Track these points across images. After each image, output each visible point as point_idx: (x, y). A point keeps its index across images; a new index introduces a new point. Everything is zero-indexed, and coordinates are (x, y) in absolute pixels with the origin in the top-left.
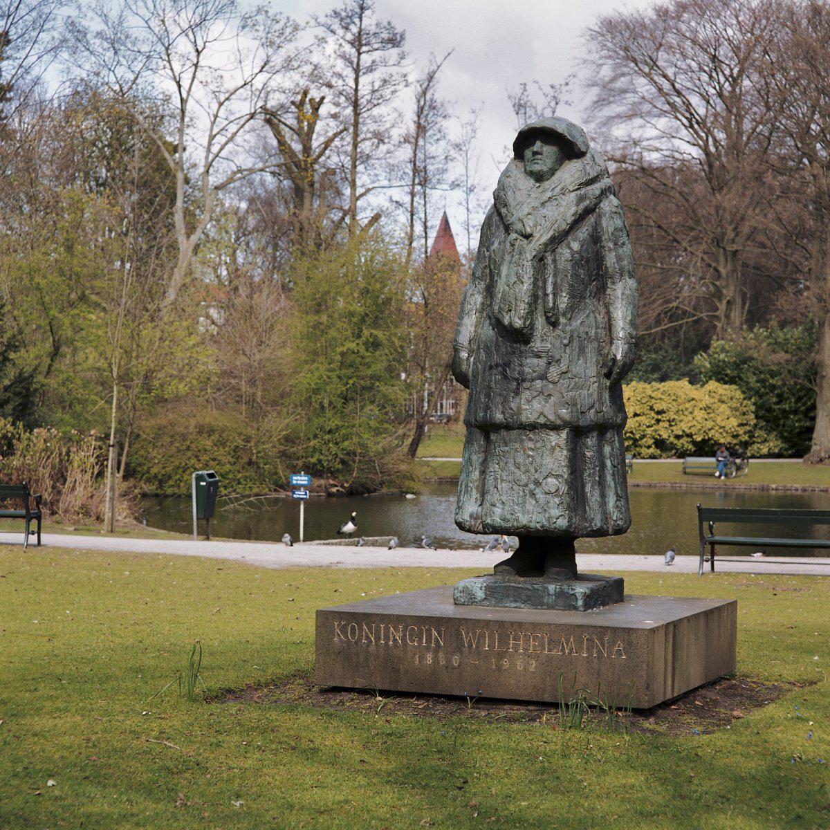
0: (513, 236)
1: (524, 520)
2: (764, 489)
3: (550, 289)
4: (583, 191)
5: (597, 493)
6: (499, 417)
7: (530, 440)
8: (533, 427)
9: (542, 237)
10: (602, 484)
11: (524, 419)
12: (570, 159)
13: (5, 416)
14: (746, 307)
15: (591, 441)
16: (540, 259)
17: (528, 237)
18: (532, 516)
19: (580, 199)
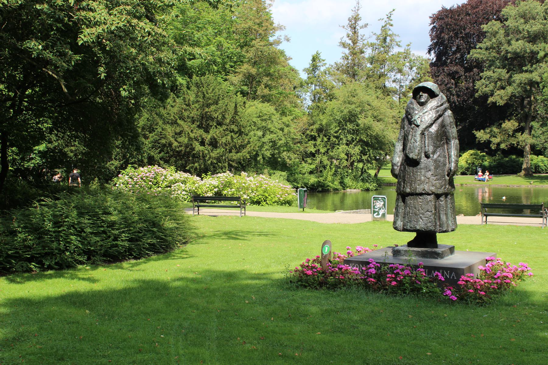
0: (413, 126)
1: (418, 228)
2: (12, 281)
3: (427, 144)
4: (438, 109)
5: (445, 217)
6: (408, 190)
7: (420, 199)
8: (421, 194)
9: (423, 127)
10: (446, 214)
11: (417, 192)
12: (432, 98)
13: (3, 83)
14: (250, 282)
15: (442, 198)
16: (423, 134)
17: (418, 126)
18: (421, 225)
19: (438, 112)
